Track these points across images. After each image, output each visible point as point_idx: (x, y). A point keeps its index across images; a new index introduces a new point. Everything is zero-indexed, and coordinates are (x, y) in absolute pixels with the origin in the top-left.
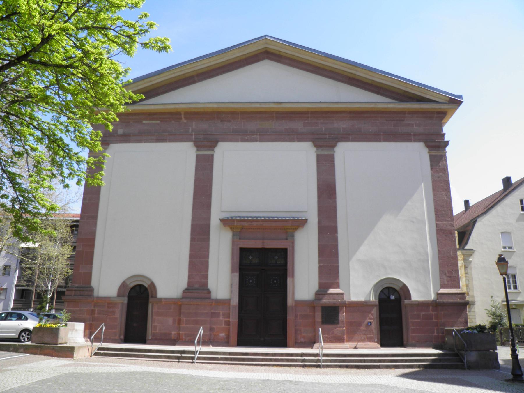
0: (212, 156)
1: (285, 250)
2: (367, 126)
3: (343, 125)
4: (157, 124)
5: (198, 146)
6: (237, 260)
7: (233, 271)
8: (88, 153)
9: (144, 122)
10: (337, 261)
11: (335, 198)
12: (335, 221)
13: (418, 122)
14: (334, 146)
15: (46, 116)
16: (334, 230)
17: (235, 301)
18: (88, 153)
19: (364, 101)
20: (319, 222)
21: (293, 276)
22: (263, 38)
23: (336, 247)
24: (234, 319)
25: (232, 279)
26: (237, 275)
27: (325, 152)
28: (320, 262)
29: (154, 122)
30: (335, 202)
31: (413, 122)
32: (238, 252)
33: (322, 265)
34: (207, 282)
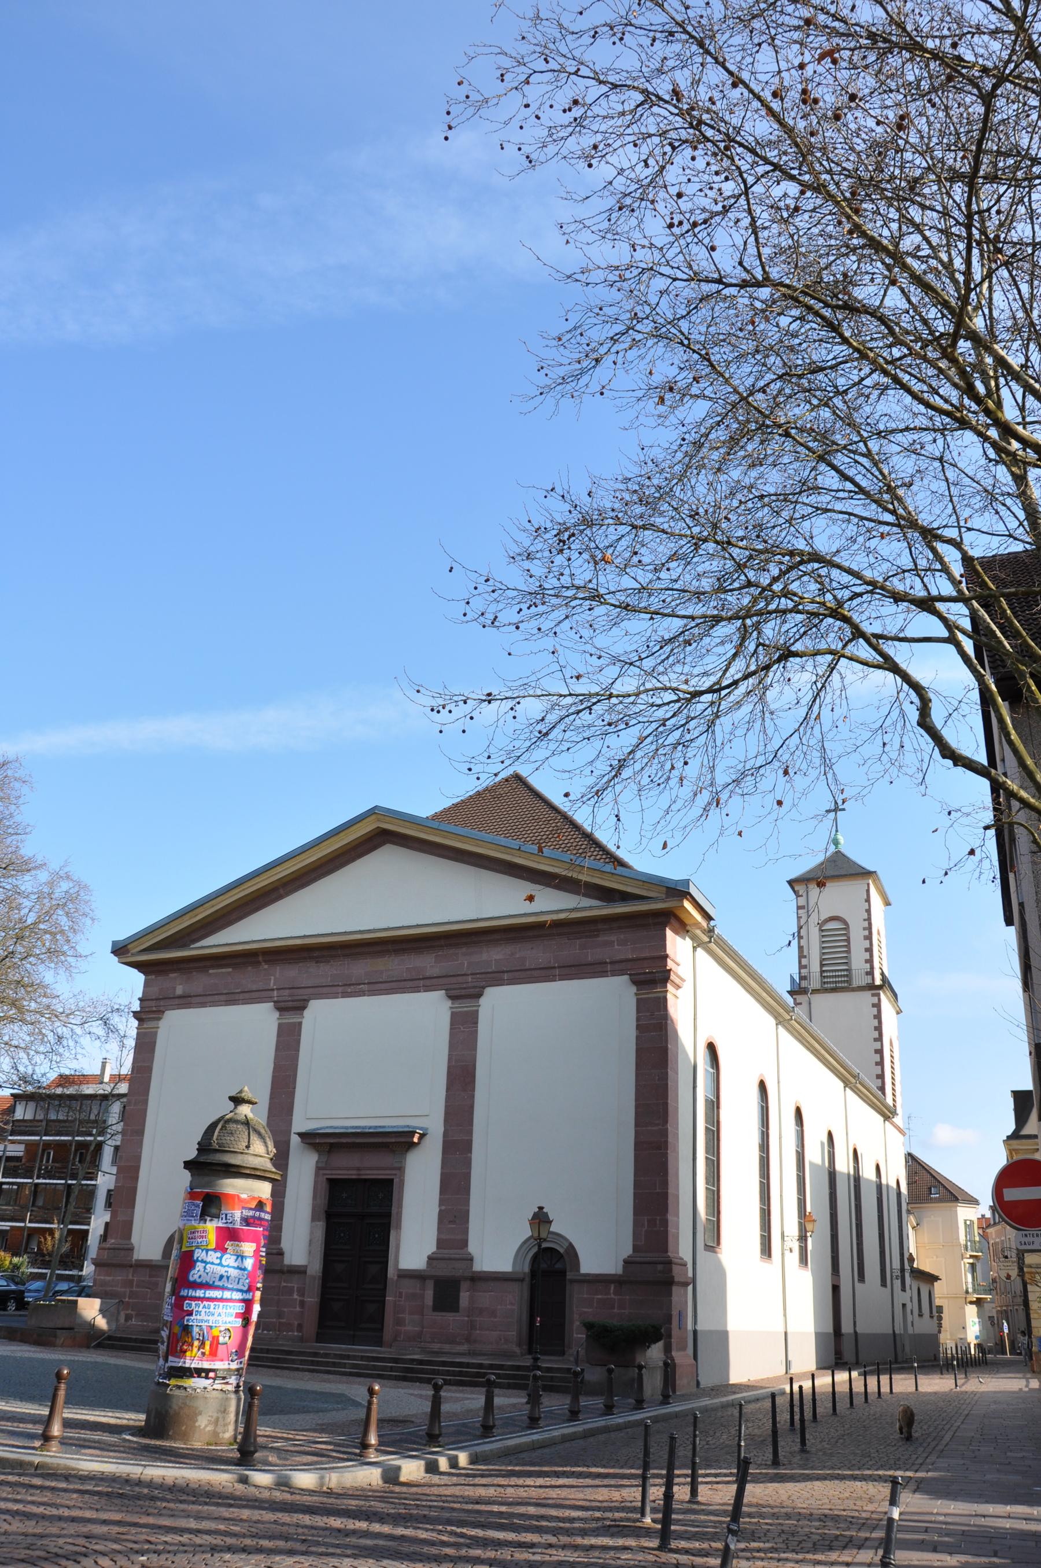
0: (300, 1024)
1: (390, 1182)
2: (535, 954)
3: (495, 955)
4: (229, 973)
5: (282, 1008)
6: (323, 1201)
7: (314, 1218)
8: (140, 999)
9: (211, 971)
10: (467, 1202)
11: (473, 1090)
12: (470, 1132)
13: (622, 937)
14: (479, 995)
15: (233, 1094)
16: (467, 1146)
17: (316, 1268)
18: (140, 999)
19: (507, 914)
20: (446, 1134)
21: (399, 1227)
22: (373, 812)
23: (467, 1176)
24: (313, 1299)
25: (312, 1233)
26: (321, 1226)
27: (465, 1006)
28: (441, 1202)
29: (224, 970)
30: (473, 1097)
31: (613, 938)
32: (324, 1186)
33: (443, 1208)
34: (280, 1236)
